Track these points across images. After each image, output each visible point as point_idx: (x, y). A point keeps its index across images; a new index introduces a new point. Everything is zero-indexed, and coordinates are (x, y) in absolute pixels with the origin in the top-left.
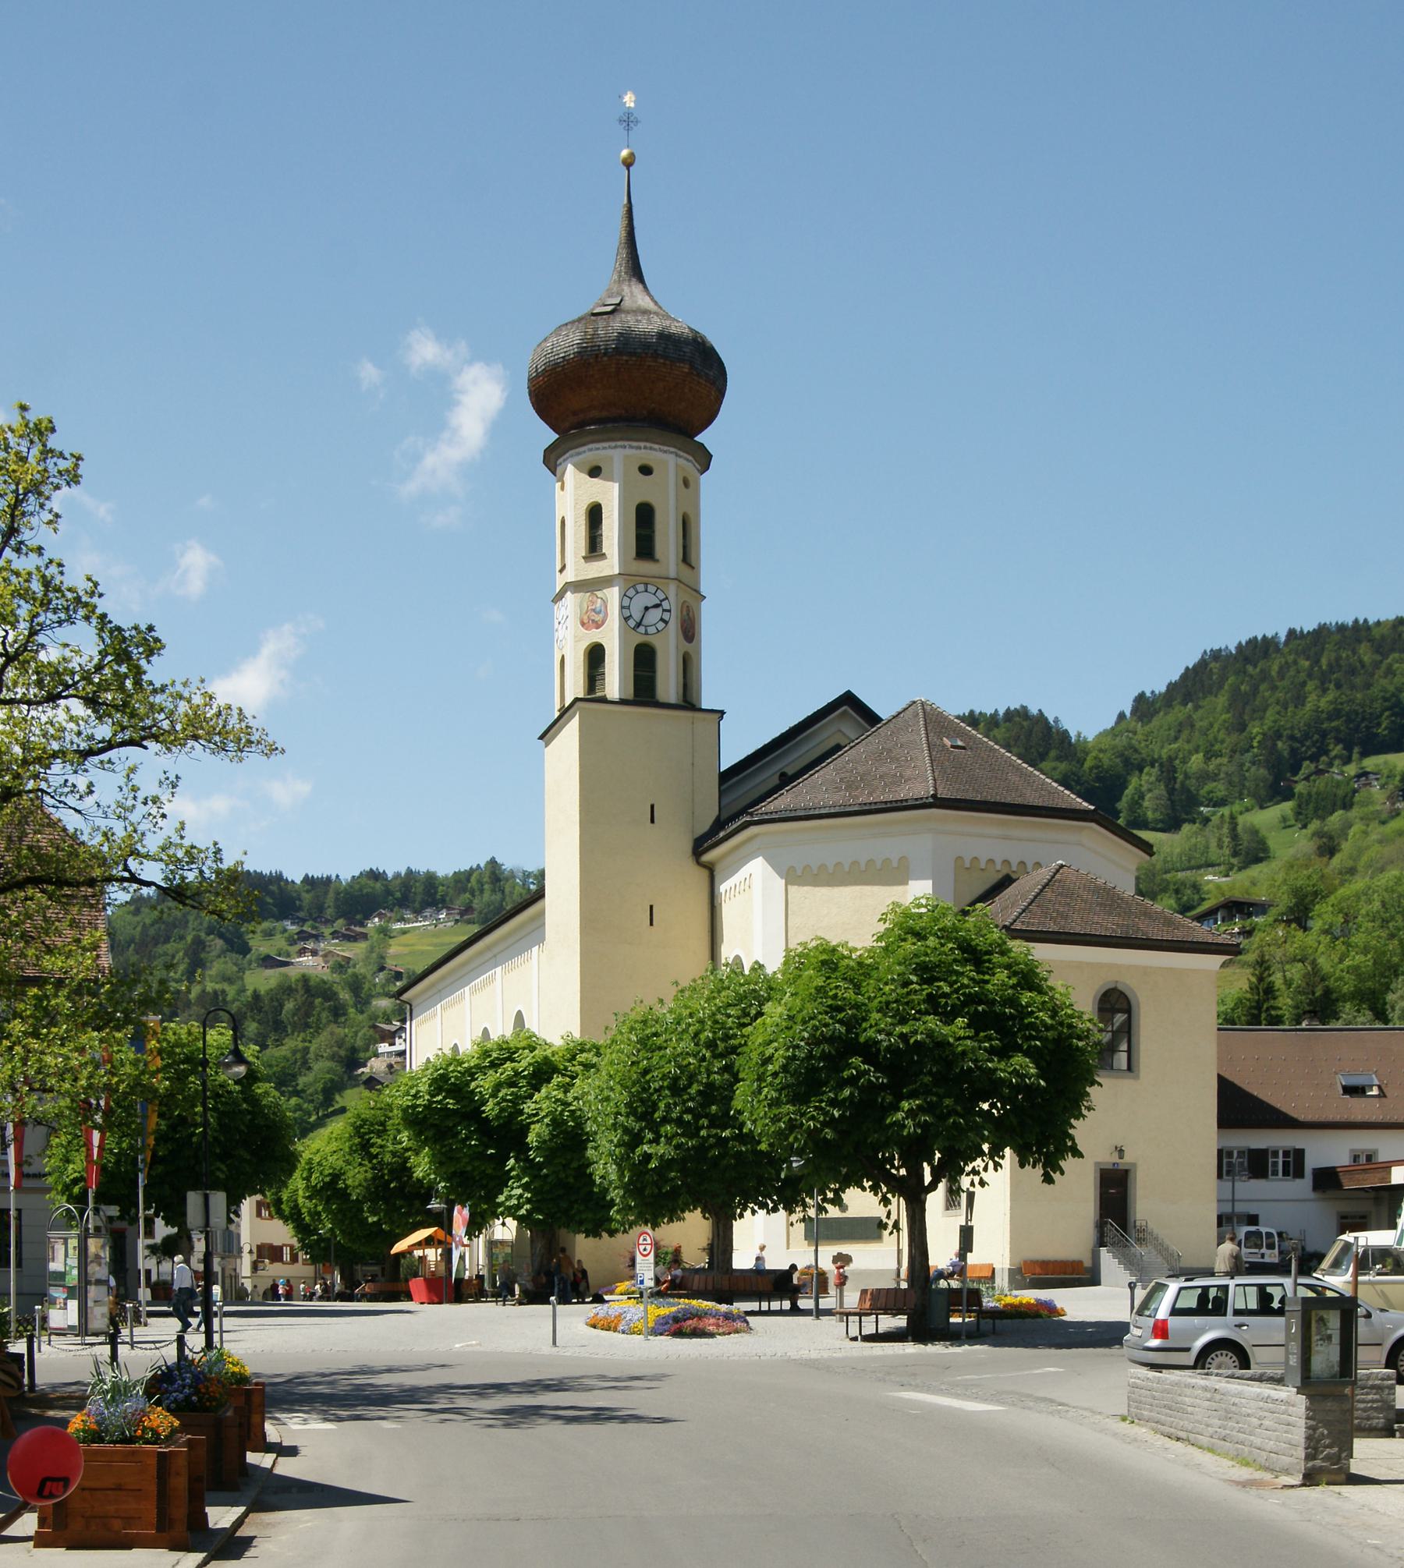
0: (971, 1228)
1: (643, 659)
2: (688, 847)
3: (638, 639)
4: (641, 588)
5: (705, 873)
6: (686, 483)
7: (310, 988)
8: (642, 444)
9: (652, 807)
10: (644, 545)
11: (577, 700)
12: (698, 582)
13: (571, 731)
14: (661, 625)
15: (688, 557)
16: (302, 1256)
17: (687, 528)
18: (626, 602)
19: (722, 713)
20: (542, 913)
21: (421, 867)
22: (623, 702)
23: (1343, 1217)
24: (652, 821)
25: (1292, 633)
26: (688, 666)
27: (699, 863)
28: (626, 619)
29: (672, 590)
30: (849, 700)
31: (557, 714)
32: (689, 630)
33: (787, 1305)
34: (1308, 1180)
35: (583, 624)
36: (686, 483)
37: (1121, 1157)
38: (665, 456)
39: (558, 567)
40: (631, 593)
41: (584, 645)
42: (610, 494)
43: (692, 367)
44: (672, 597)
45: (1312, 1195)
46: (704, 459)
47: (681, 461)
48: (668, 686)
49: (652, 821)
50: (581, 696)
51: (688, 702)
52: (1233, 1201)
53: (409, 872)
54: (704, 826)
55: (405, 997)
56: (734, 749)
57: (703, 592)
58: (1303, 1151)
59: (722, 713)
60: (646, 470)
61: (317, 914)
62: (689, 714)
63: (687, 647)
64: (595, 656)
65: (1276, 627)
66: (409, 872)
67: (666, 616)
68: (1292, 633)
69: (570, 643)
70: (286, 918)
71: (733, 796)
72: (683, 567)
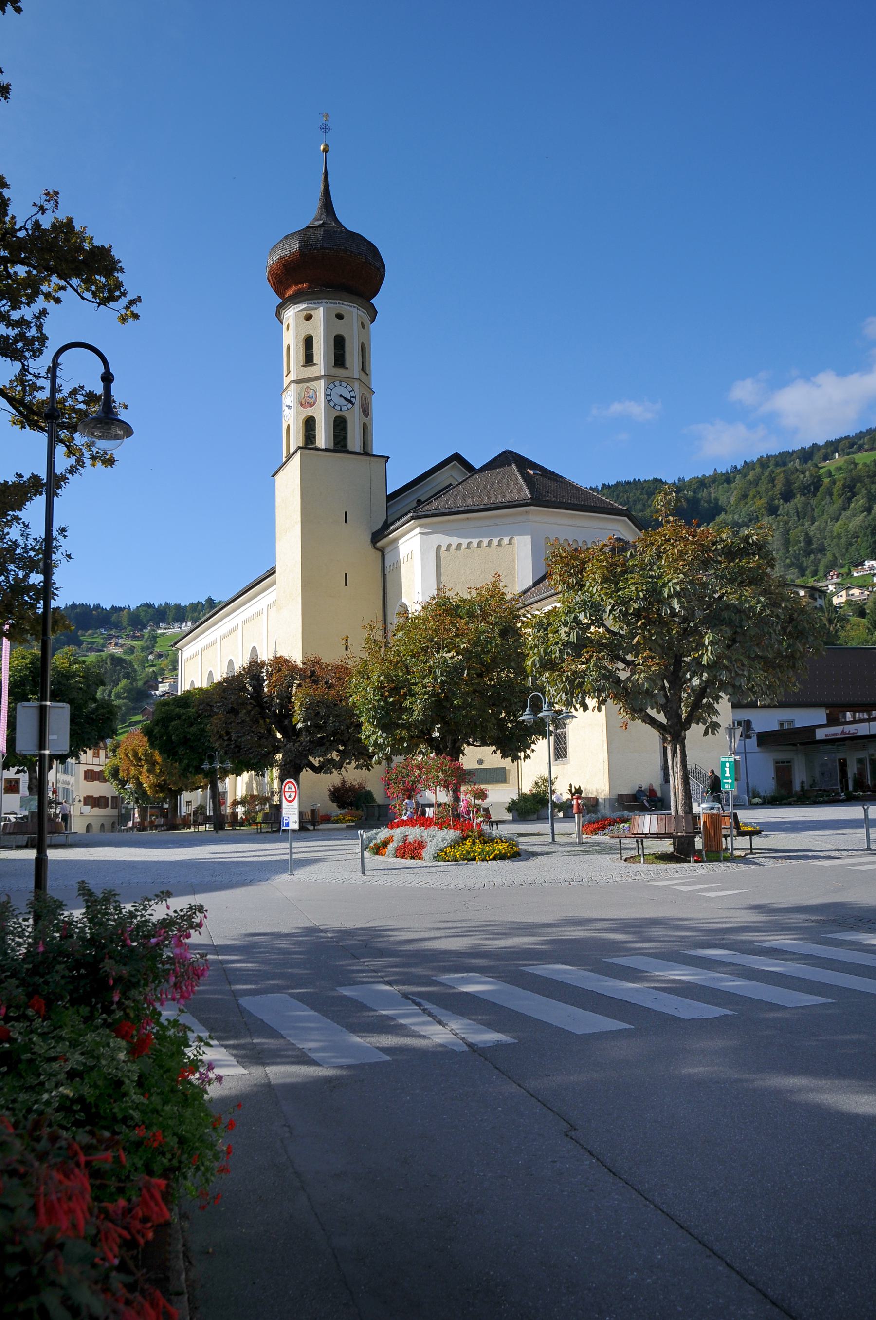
1: (339, 425)
2: (368, 538)
3: (338, 413)
4: (337, 383)
5: (379, 554)
6: (363, 326)
7: (117, 661)
8: (337, 302)
9: (346, 513)
10: (339, 358)
11: (299, 448)
12: (370, 383)
15: (364, 368)
17: (363, 349)
18: (329, 392)
19: (388, 458)
21: (173, 602)
22: (326, 450)
23: (777, 763)
24: (346, 522)
25: (604, 485)
26: (366, 429)
27: (375, 548)
28: (329, 401)
29: (356, 385)
30: (457, 457)
31: (284, 460)
32: (366, 411)
34: (755, 739)
35: (302, 405)
36: (363, 326)
38: (351, 309)
39: (285, 373)
40: (332, 386)
41: (303, 417)
42: (318, 328)
45: (757, 749)
46: (373, 314)
47: (360, 313)
48: (354, 442)
49: (346, 522)
51: (366, 452)
53: (167, 604)
54: (378, 526)
55: (178, 646)
59: (388, 458)
60: (340, 316)
61: (117, 626)
62: (367, 458)
63: (366, 420)
64: (309, 424)
66: (167, 604)
68: (604, 485)
69: (291, 418)
70: (102, 628)
72: (362, 373)
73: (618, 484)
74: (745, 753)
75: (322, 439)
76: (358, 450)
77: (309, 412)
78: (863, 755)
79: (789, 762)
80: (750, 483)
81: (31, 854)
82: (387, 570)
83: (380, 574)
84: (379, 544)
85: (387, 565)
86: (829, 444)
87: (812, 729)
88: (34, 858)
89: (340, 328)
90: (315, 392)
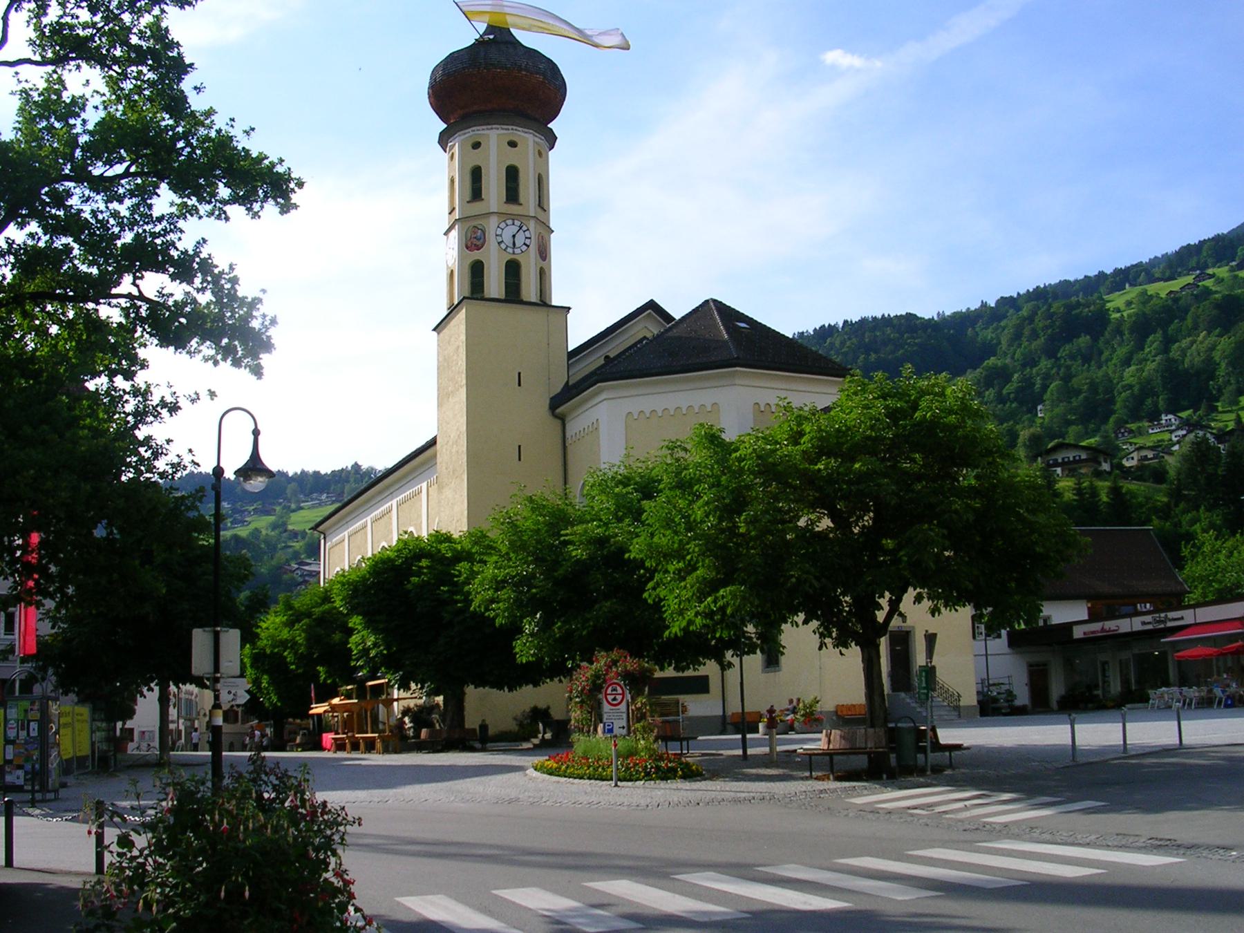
0: (934, 668)
1: (513, 270)
5: (558, 422)
6: (540, 154)
13: (462, 315)
14: (524, 248)
16: (30, 242)
17: (542, 183)
19: (569, 308)
20: (435, 456)
25: (846, 322)
26: (544, 276)
30: (652, 306)
32: (544, 253)
33: (807, 774)
36: (540, 154)
37: (904, 621)
41: (469, 261)
43: (545, 77)
44: (532, 229)
46: (551, 139)
48: (529, 291)
50: (467, 295)
51: (543, 302)
52: (986, 655)
55: (321, 528)
56: (579, 332)
57: (552, 226)
58: (935, 635)
59: (569, 308)
60: (513, 144)
62: (545, 309)
63: (543, 264)
65: (837, 319)
67: (528, 242)
68: (846, 322)
71: (578, 367)
72: (539, 210)
73: (863, 321)
74: (986, 655)
75: (495, 284)
76: (533, 299)
77: (476, 255)
78: (1125, 655)
79: (1045, 665)
80: (1025, 319)
81: (739, 736)
82: (569, 441)
83: (560, 447)
84: (558, 411)
85: (568, 435)
86: (1118, 272)
87: (1068, 627)
88: (975, 703)
89: (513, 157)
90: (484, 232)
